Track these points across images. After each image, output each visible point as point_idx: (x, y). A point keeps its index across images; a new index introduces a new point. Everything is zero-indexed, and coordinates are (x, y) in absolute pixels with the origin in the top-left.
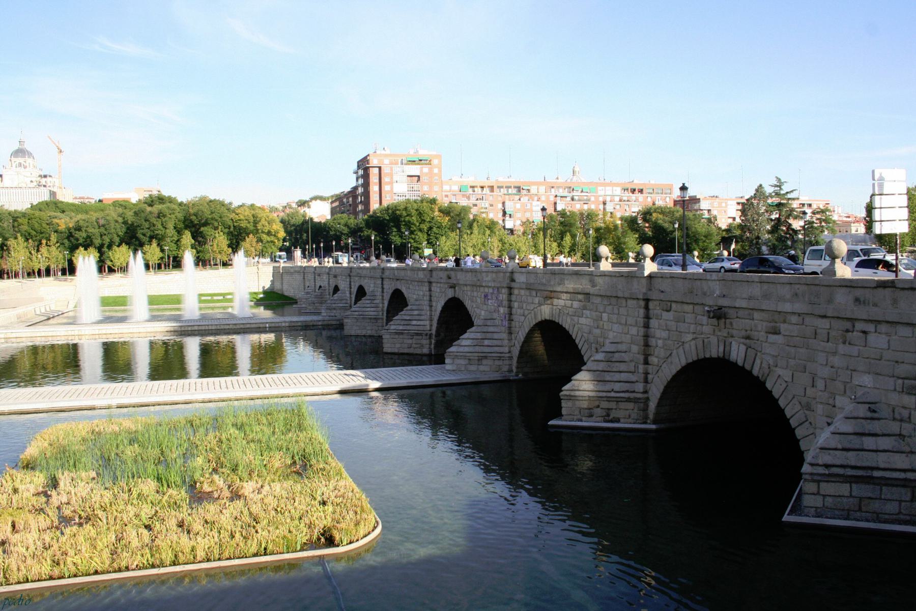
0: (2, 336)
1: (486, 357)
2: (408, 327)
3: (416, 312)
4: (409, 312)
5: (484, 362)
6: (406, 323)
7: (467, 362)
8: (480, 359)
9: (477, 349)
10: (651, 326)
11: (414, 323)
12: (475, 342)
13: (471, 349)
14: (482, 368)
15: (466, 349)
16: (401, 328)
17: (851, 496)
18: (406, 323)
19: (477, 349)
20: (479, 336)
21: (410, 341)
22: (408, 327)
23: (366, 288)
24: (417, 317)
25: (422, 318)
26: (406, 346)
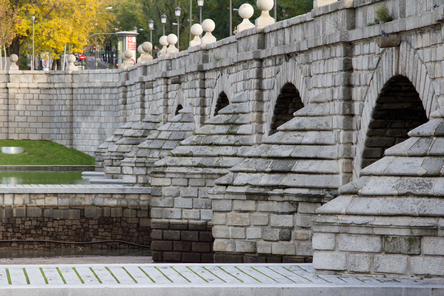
0: (1, 230)
1: (432, 231)
2: (286, 180)
3: (310, 137)
4: (292, 137)
5: (429, 245)
6: (279, 165)
7: (375, 244)
8: (414, 242)
9: (411, 205)
10: (355, 66)
11: (300, 166)
12: (407, 185)
13: (391, 206)
14: (421, 265)
15: (377, 206)
16: (265, 180)
17: (30, 104)
18: (279, 165)
19: (411, 205)
20: (419, 166)
21: (287, 221)
22: (286, 180)
23: (424, 89)
24: (311, 151)
25: (325, 152)
26: (276, 234)
